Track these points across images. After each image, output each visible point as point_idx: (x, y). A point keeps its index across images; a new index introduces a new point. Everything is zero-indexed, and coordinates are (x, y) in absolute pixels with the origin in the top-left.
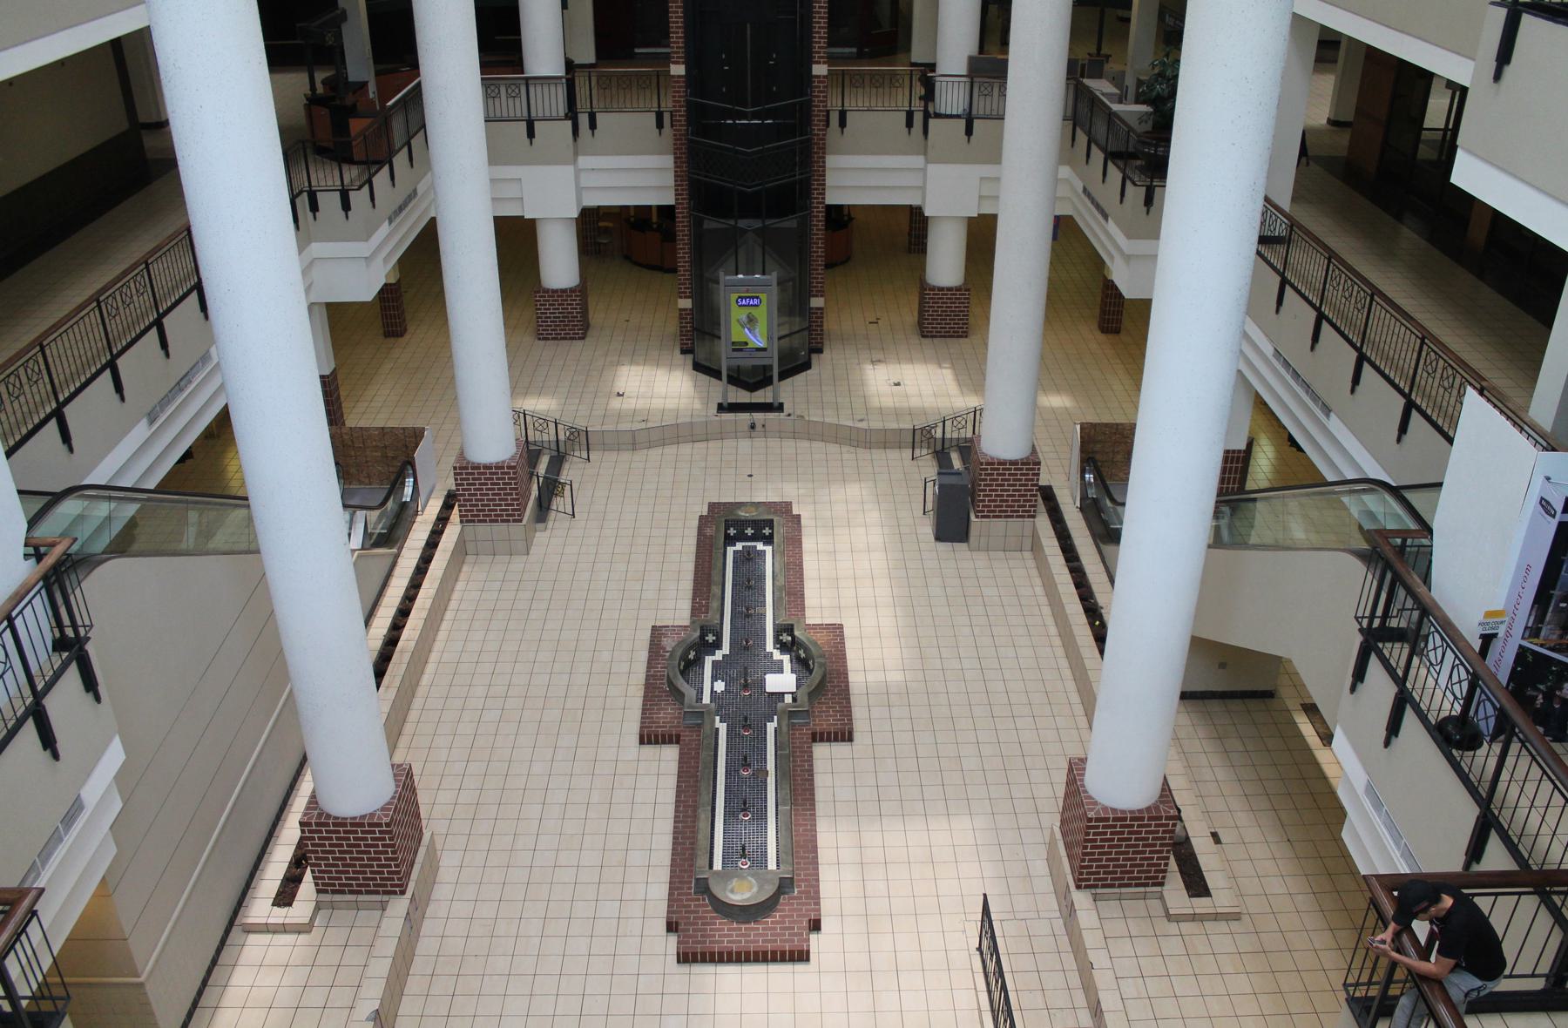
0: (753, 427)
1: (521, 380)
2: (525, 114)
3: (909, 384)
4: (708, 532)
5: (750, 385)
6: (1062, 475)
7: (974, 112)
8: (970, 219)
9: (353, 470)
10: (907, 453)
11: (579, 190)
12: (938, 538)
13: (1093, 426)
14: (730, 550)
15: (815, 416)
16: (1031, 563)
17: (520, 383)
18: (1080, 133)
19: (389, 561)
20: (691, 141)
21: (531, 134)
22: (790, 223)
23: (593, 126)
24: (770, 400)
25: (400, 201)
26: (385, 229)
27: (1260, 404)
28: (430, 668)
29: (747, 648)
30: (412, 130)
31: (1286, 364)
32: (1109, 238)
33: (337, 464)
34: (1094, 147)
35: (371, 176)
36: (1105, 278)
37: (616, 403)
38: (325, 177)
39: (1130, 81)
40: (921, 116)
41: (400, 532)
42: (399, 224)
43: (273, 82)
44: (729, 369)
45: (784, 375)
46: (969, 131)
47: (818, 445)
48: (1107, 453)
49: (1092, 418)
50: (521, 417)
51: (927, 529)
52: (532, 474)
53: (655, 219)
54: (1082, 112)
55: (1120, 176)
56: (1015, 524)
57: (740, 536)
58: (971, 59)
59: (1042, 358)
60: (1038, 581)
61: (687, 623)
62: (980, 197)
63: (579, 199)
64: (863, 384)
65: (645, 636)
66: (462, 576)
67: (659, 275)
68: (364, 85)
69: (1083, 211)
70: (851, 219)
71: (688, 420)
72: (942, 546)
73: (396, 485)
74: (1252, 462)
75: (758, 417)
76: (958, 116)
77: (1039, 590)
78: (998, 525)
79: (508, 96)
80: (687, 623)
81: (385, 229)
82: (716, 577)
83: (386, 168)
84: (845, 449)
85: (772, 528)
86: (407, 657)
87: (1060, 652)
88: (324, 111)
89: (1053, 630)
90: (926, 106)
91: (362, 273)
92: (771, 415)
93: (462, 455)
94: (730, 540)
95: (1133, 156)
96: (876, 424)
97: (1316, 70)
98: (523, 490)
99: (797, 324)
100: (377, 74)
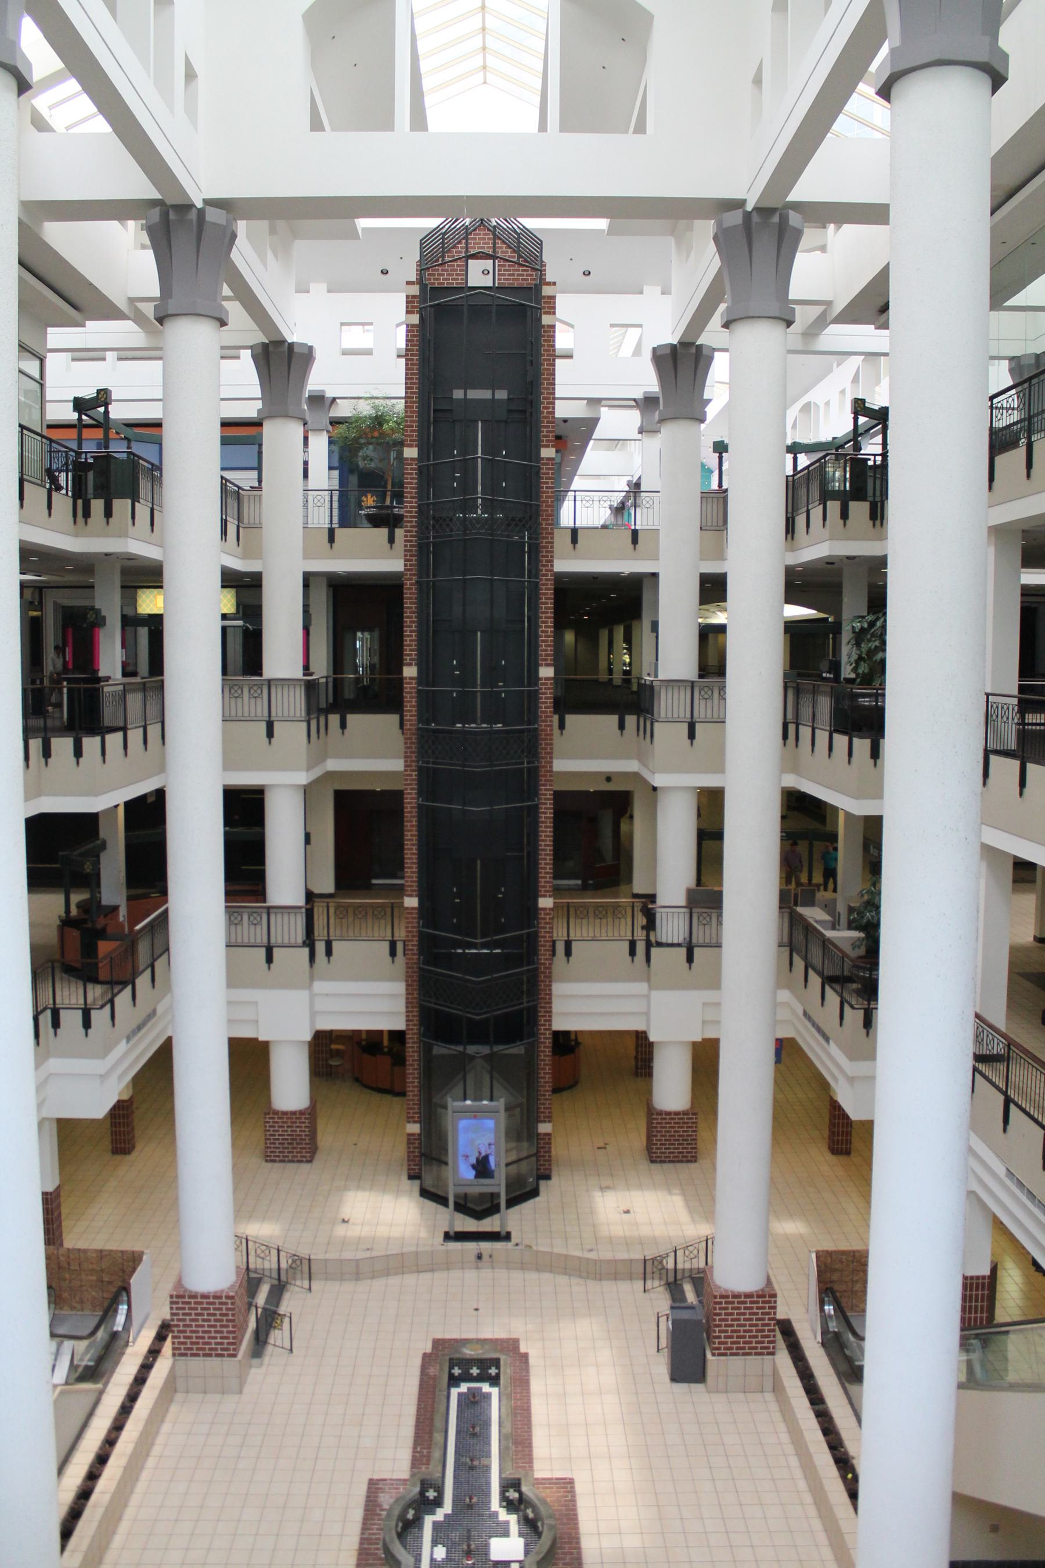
0: (479, 1257)
1: (245, 1201)
2: (265, 940)
3: (634, 1210)
4: (432, 1371)
5: (479, 1211)
6: (800, 1307)
7: (694, 941)
8: (695, 1045)
9: (65, 1295)
10: (640, 1284)
11: (313, 1014)
12: (674, 1379)
13: (829, 1254)
14: (454, 1392)
15: (543, 1246)
16: (774, 1406)
17: (244, 1206)
18: (796, 957)
19: (92, 1399)
20: (421, 969)
21: (269, 959)
22: (517, 1049)
23: (329, 952)
24: (497, 1229)
25: (139, 1021)
26: (122, 1047)
27: (998, 1225)
28: (124, 1527)
29: (470, 1506)
30: (157, 952)
31: (1020, 1184)
32: (831, 1059)
33: (49, 1287)
34: (811, 972)
35: (114, 996)
36: (831, 1098)
37: (340, 1231)
38: (70, 994)
39: (841, 908)
40: (645, 944)
41: (107, 1365)
42: (139, 1041)
43: (30, 902)
44: (456, 1196)
45: (511, 1203)
46: (690, 959)
47: (546, 1276)
48: (842, 1281)
49: (829, 1246)
50: (244, 1242)
51: (661, 1368)
52: (250, 1305)
53: (386, 1042)
54: (797, 939)
55: (838, 999)
56: (753, 1362)
57: (465, 1373)
58: (690, 893)
59: (772, 1181)
60: (782, 1427)
61: (406, 1475)
62: (704, 1022)
63: (312, 1022)
64: (592, 1212)
65: (362, 1490)
66: (170, 1417)
67: (388, 1098)
68: (115, 909)
69: (802, 1030)
70: (578, 1044)
71: (413, 1249)
72: (681, 1388)
73: (109, 1311)
74: (998, 1287)
75: (485, 1246)
76: (679, 945)
77: (785, 1438)
78: (736, 1364)
79: (251, 923)
80: (406, 1475)
81: (122, 1047)
82: (438, 1423)
83: (129, 988)
84: (575, 1280)
85: (498, 1367)
86: (100, 1512)
87: (812, 1511)
88: (76, 933)
89: (802, 1485)
90: (648, 935)
91: (95, 1087)
92: (498, 1245)
93: (179, 1283)
94: (454, 1381)
95: (849, 980)
96: (606, 1255)
97: (1015, 890)
98: (237, 1322)
99: (526, 1148)
100: (129, 898)
